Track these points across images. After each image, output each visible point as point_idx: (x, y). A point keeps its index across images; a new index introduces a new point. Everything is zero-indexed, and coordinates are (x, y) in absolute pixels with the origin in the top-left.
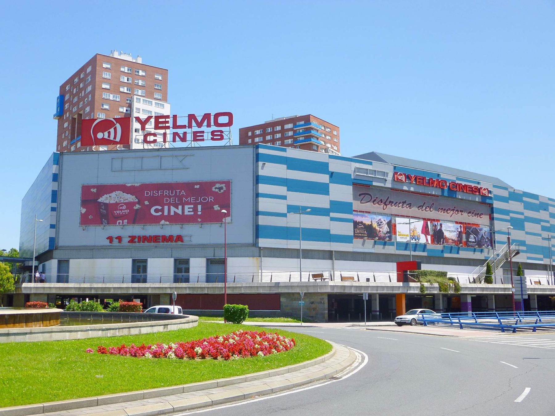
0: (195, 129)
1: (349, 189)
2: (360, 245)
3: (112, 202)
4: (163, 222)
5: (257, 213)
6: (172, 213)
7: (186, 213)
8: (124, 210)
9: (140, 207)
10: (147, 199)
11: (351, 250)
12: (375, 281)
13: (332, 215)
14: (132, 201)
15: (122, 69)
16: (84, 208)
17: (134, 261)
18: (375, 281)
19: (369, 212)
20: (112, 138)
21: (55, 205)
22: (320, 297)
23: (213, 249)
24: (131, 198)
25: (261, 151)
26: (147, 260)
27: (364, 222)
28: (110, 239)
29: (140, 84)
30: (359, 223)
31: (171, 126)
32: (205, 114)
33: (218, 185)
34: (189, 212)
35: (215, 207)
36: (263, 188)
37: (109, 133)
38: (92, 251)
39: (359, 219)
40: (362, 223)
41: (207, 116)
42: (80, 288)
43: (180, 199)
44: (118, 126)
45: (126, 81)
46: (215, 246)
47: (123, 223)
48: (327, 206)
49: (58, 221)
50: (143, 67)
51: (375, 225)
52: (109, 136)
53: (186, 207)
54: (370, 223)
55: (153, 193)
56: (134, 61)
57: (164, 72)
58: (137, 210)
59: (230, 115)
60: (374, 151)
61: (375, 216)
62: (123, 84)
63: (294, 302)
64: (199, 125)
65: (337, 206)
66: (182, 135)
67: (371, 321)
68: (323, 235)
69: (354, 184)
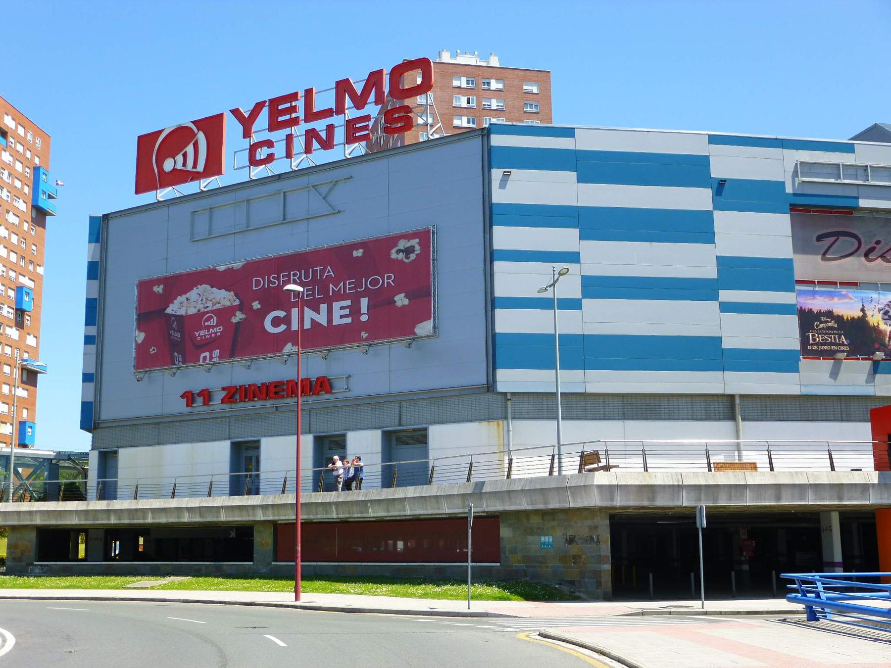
0: (351, 113)
1: (782, 222)
2: (825, 376)
3: (192, 311)
4: (289, 348)
5: (492, 303)
6: (307, 325)
7: (337, 321)
8: (213, 327)
9: (243, 316)
10: (256, 296)
11: (795, 390)
12: (772, 469)
13: (726, 295)
14: (228, 304)
15: (456, 83)
16: (140, 331)
17: (233, 444)
18: (772, 469)
19: (855, 284)
20: (190, 167)
21: (93, 331)
22: (588, 523)
23: (397, 405)
24: (225, 298)
25: (497, 140)
26: (258, 442)
27: (838, 311)
28: (190, 398)
29: (494, 107)
30: (820, 314)
31: (302, 117)
32: (371, 74)
33: (402, 244)
34: (342, 317)
35: (397, 298)
36: (505, 237)
37: (185, 156)
38: (157, 429)
39: (818, 304)
40: (829, 314)
41: (374, 78)
42: (86, 512)
43: (323, 286)
44: (201, 137)
45: (464, 104)
46: (403, 399)
47: (211, 358)
48: (711, 273)
49: (99, 363)
50: (499, 73)
51: (875, 318)
52: (184, 164)
53: (336, 305)
54: (858, 314)
55: (269, 282)
56: (484, 64)
57: (542, 76)
58: (238, 323)
59: (423, 64)
60: (880, 121)
61: (874, 295)
62: (460, 111)
63: (530, 538)
64: (360, 102)
65: (738, 271)
66: (323, 135)
67: (733, 597)
68: (705, 353)
69: (795, 209)
